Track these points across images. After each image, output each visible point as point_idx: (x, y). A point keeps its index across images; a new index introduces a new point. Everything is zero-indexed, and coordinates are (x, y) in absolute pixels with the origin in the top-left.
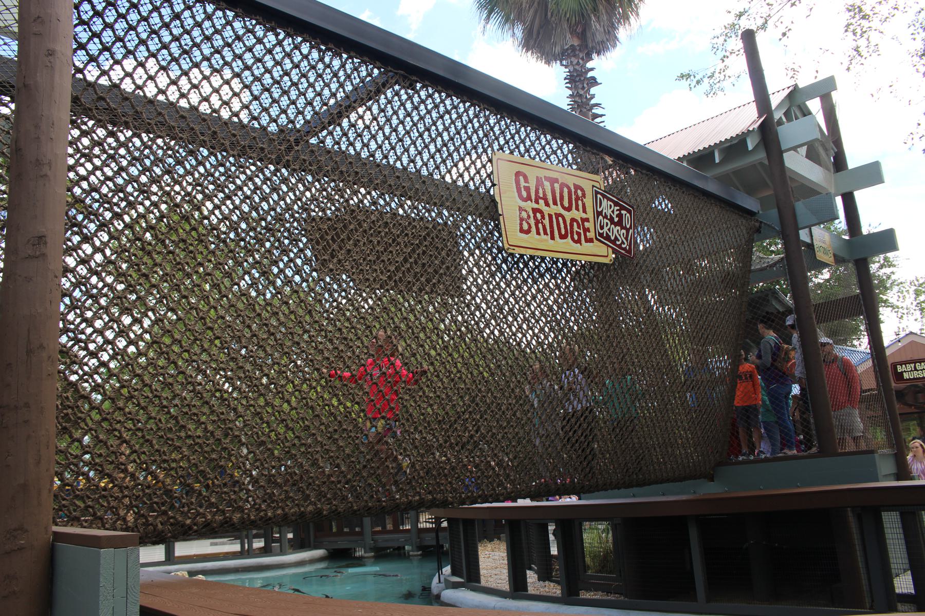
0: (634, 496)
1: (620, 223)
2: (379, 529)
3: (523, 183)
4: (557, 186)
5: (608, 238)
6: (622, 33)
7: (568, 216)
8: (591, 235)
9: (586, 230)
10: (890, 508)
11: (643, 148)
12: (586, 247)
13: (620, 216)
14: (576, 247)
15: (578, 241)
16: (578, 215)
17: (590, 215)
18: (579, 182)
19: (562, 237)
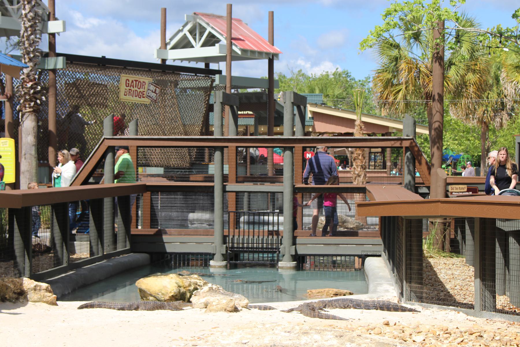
0: (402, 234)
1: (155, 92)
2: (239, 149)
3: (128, 82)
4: (137, 82)
5: (150, 97)
6: (101, 57)
7: (139, 90)
8: (144, 96)
9: (143, 94)
10: (107, 196)
11: (227, 24)
12: (142, 99)
13: (155, 90)
14: (139, 99)
15: (140, 98)
16: (141, 90)
17: (146, 90)
18: (144, 80)
19: (136, 96)
